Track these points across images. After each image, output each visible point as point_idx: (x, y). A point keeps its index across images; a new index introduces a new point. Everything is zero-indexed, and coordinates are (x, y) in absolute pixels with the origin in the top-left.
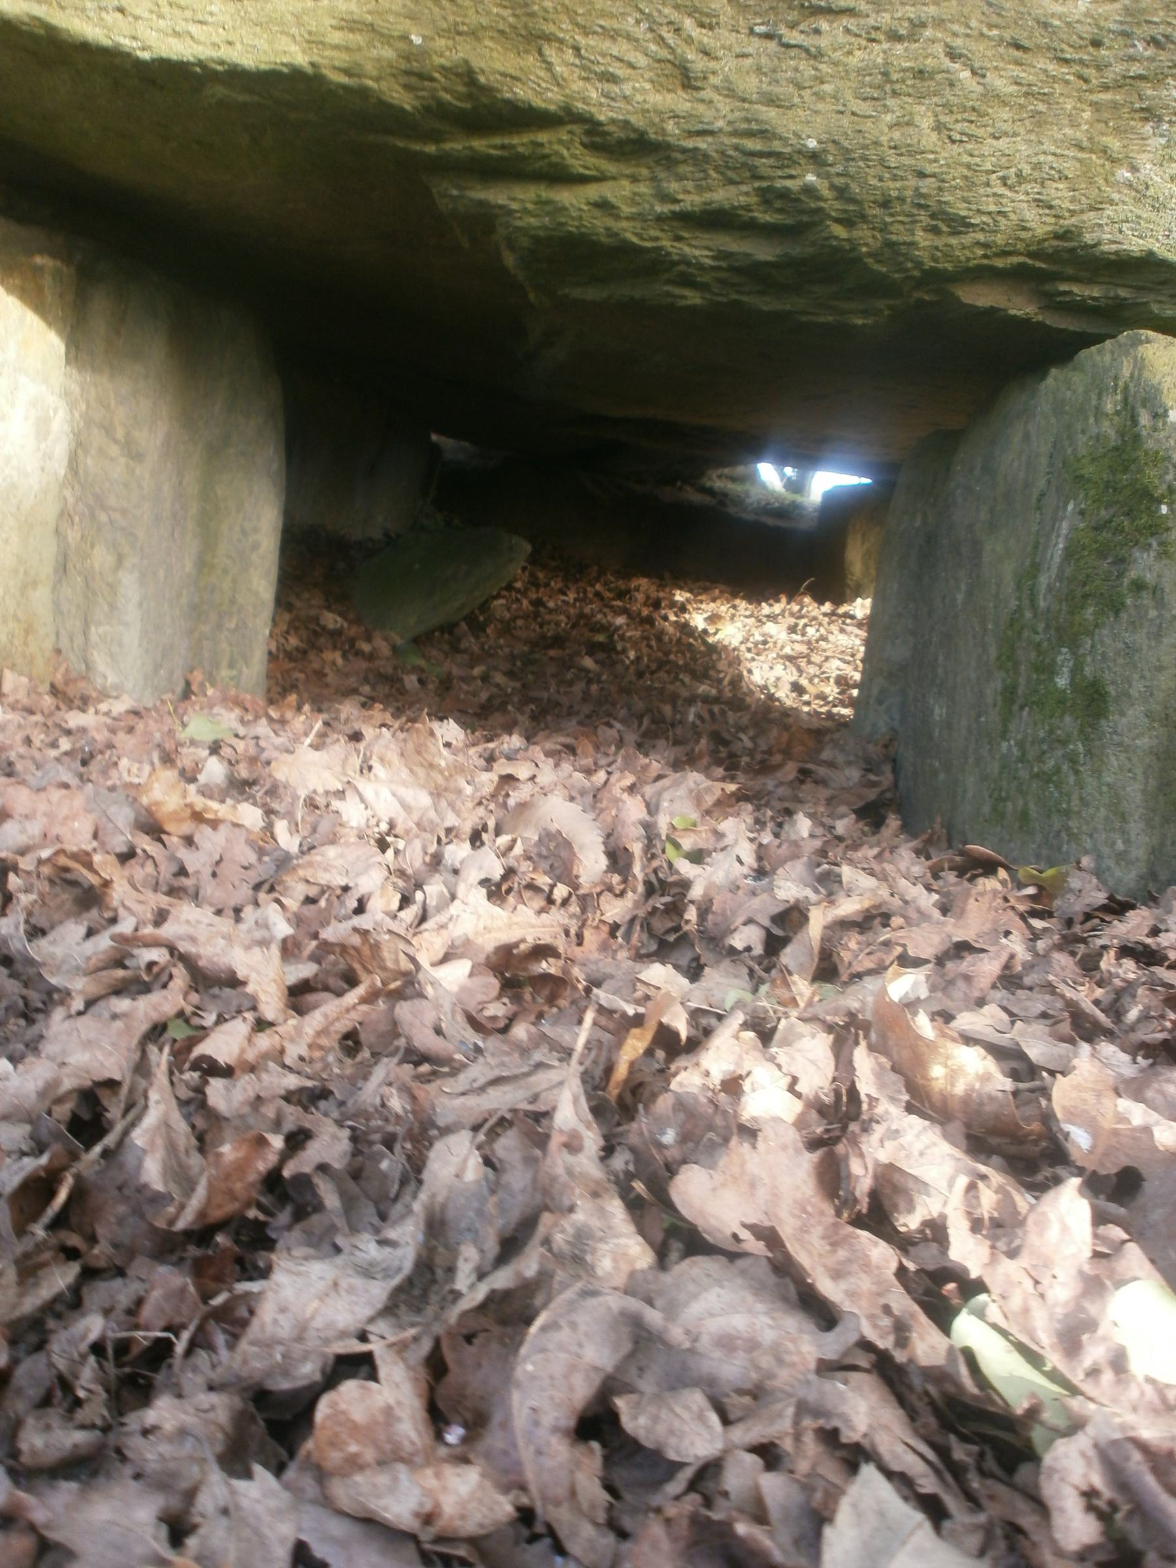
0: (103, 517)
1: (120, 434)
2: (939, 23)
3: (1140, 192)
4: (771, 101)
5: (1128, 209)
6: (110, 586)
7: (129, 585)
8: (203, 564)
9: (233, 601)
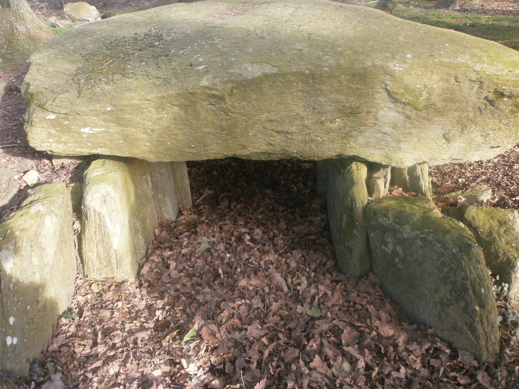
0: (158, 188)
1: (157, 171)
2: (314, 132)
3: (351, 147)
4: (286, 146)
5: (350, 149)
6: (164, 201)
7: (168, 200)
8: (175, 182)
9: (183, 187)
